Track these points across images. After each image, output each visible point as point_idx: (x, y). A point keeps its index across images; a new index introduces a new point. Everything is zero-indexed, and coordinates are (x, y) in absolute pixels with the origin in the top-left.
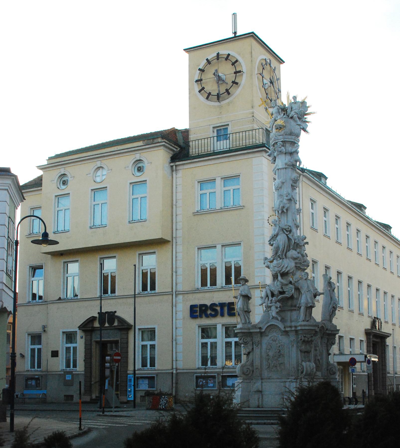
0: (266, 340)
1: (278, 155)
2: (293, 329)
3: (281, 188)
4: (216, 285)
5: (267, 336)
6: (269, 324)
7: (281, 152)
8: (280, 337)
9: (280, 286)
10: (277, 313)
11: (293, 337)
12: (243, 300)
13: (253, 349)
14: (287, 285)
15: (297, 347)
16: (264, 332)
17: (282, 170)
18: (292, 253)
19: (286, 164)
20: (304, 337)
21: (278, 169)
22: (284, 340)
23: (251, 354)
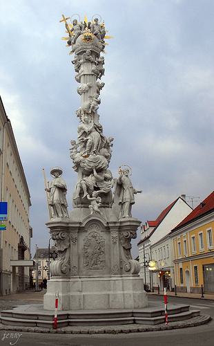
0: (83, 238)
1: (84, 62)
2: (118, 225)
3: (87, 91)
4: (6, 214)
5: (86, 231)
6: (91, 219)
7: (88, 61)
8: (102, 234)
9: (94, 182)
10: (99, 207)
11: (115, 234)
12: (59, 193)
13: (70, 246)
14: (102, 181)
15: (120, 243)
16: (83, 227)
17: (88, 77)
18: (104, 150)
19: (93, 71)
20: (131, 233)
21: (84, 75)
22: (104, 236)
23: (68, 250)
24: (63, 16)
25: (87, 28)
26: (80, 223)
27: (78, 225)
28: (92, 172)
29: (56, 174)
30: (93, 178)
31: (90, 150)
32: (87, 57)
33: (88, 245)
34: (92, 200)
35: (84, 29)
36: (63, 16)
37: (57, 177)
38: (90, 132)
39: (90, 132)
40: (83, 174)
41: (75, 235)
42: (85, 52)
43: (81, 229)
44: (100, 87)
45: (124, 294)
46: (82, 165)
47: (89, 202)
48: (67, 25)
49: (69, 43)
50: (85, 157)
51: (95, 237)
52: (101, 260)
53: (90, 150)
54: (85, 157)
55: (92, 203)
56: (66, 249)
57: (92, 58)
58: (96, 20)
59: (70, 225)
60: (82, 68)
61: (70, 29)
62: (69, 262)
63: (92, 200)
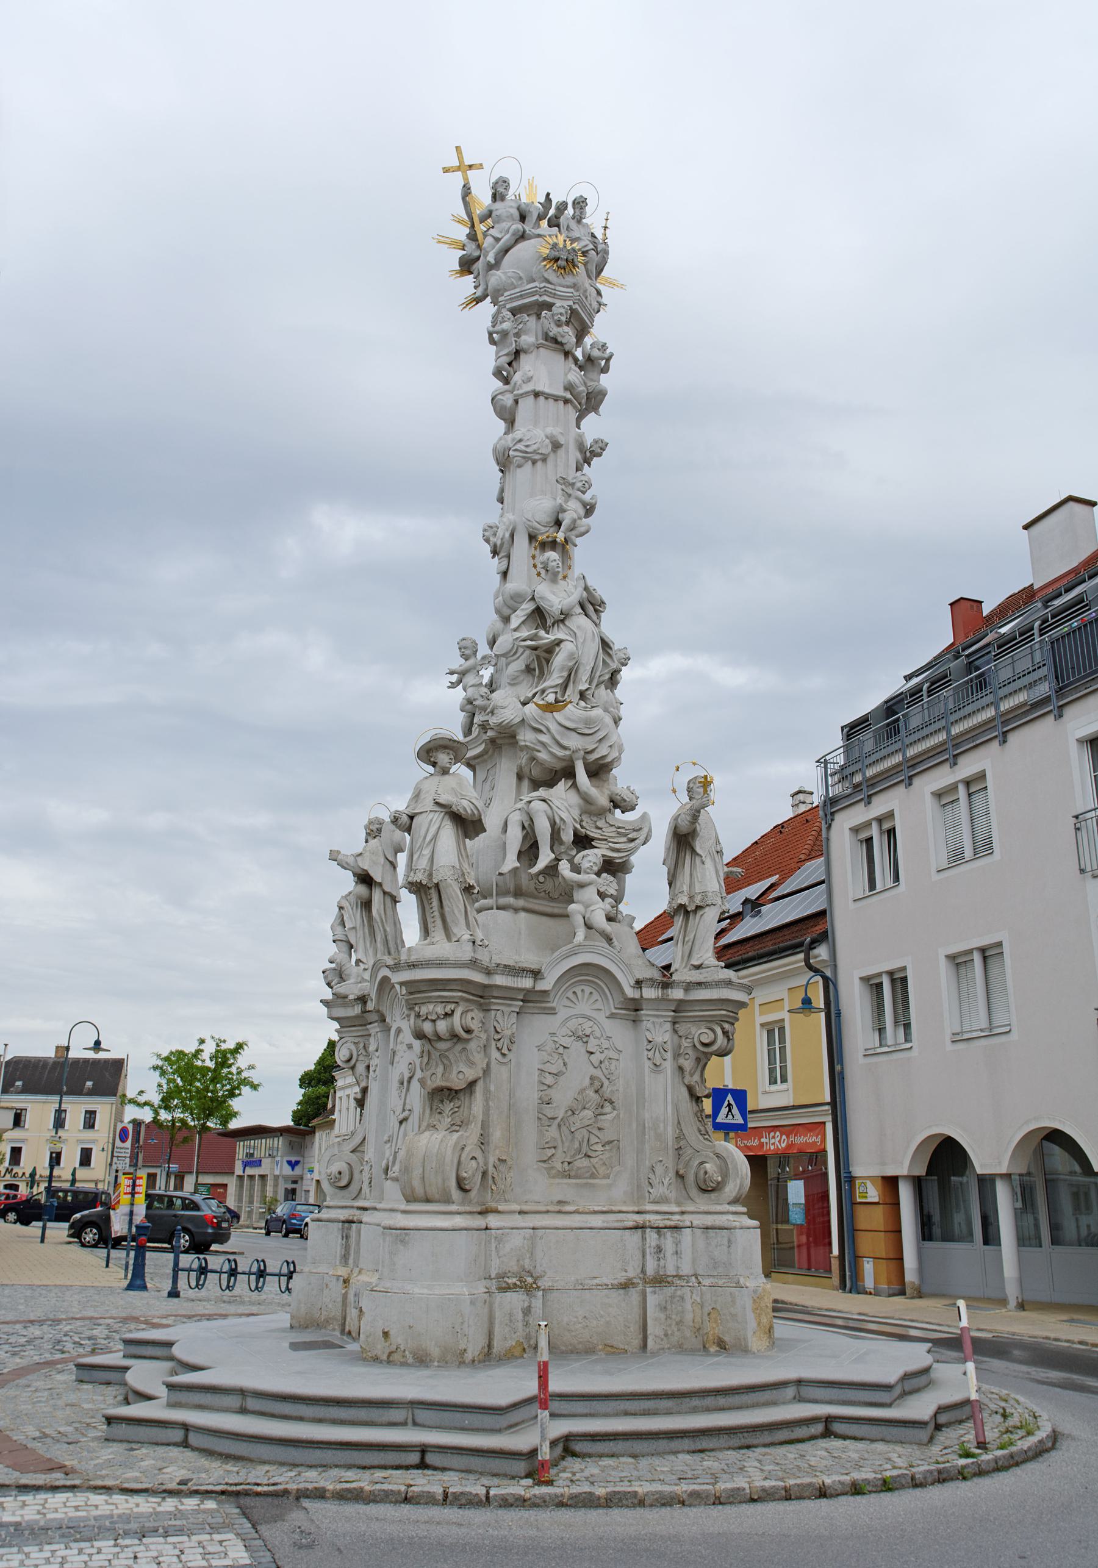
0: (536, 1034)
5: (552, 1012)
13: (487, 1071)
21: (537, 394)
23: (479, 1088)
24: (446, 170)
25: (544, 223)
26: (536, 974)
27: (527, 983)
28: (569, 773)
29: (443, 758)
30: (573, 798)
31: (565, 686)
32: (554, 331)
33: (547, 1081)
34: (582, 886)
35: (537, 225)
36: (446, 170)
37: (445, 772)
38: (564, 618)
39: (564, 618)
40: (520, 777)
41: (504, 1018)
42: (549, 306)
43: (532, 1001)
44: (589, 454)
45: (792, 1248)
46: (526, 737)
47: (567, 894)
48: (466, 191)
49: (467, 266)
50: (549, 708)
51: (583, 1038)
52: (606, 1136)
53: (565, 686)
54: (549, 708)
55: (578, 895)
56: (472, 1084)
57: (568, 335)
58: (580, 204)
59: (499, 980)
60: (527, 365)
61: (478, 212)
62: (483, 1142)
63: (582, 886)
